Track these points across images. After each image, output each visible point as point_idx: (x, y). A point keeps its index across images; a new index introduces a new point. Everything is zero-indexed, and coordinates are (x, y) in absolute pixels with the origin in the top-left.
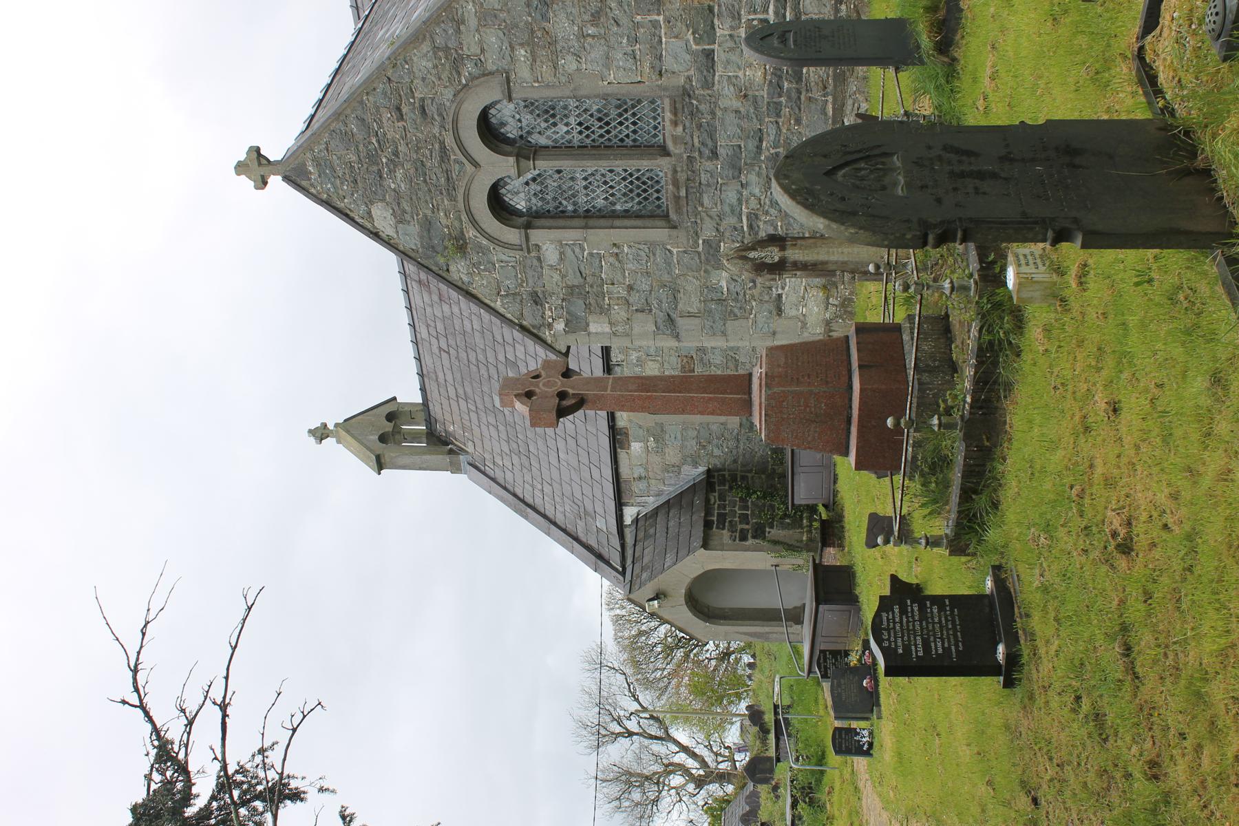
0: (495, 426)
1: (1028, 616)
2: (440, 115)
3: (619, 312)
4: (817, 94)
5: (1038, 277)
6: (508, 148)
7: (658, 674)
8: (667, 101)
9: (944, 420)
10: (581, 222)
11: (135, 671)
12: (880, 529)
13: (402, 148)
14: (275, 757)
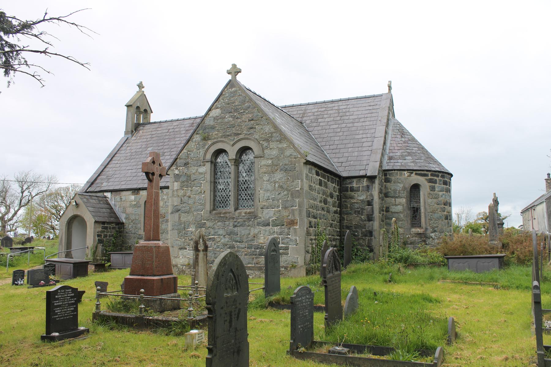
0: (143, 148)
1: (70, 343)
2: (250, 134)
3: (181, 193)
4: (255, 261)
5: (194, 341)
6: (238, 156)
7: (46, 203)
8: (253, 210)
9: (143, 310)
10: (213, 180)
11: (58, 19)
12: (102, 286)
13: (239, 120)
14: (24, 68)
